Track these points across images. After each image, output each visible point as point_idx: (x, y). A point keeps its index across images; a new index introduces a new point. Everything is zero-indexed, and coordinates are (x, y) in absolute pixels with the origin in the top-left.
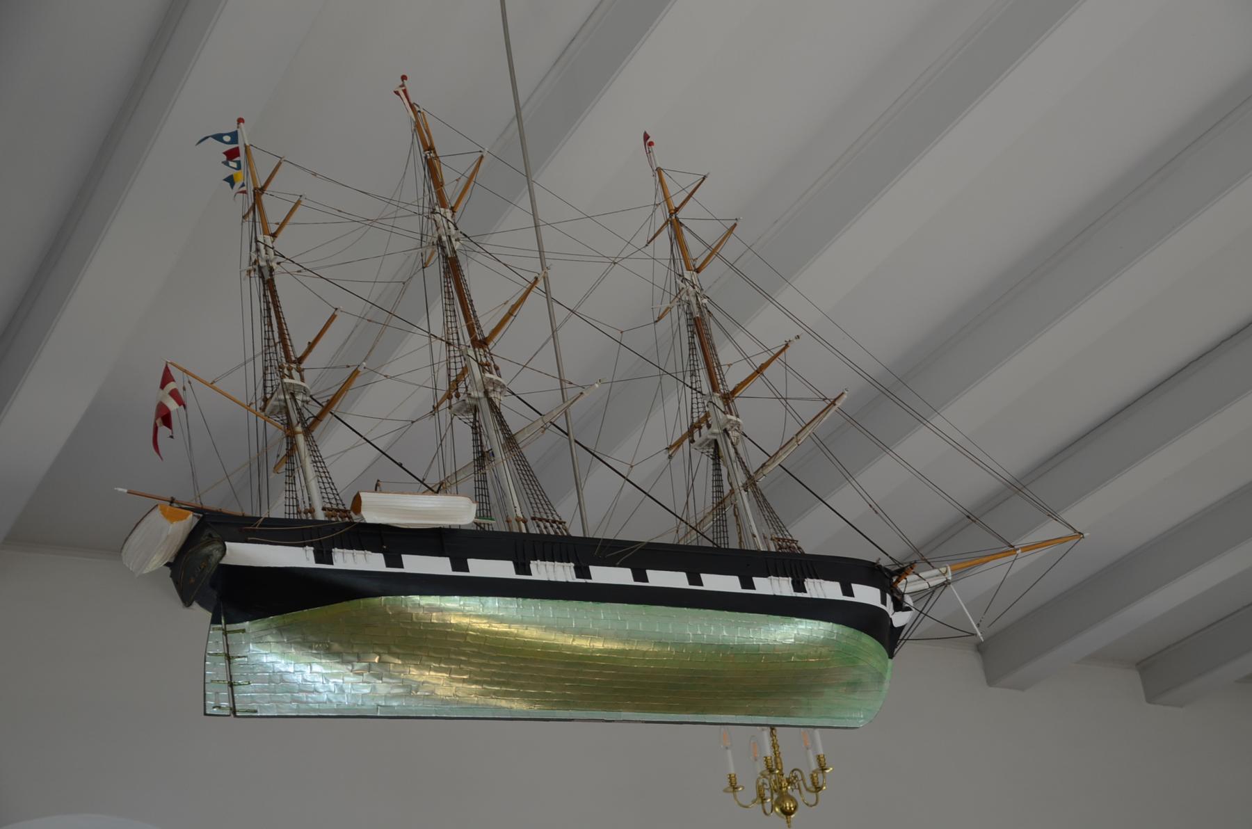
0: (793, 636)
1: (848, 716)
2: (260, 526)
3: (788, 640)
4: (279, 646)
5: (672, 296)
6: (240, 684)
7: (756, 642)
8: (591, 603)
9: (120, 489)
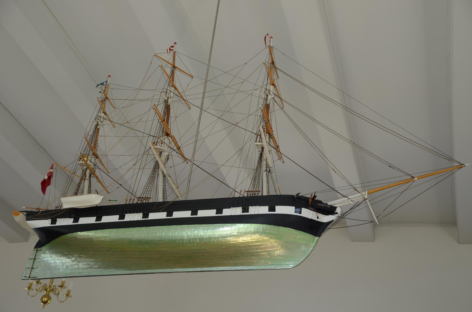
0: (236, 231)
1: (284, 264)
2: (40, 214)
3: (233, 234)
4: (50, 254)
5: (238, 92)
6: (35, 268)
7: (217, 235)
8: (144, 227)
9: (23, 207)
